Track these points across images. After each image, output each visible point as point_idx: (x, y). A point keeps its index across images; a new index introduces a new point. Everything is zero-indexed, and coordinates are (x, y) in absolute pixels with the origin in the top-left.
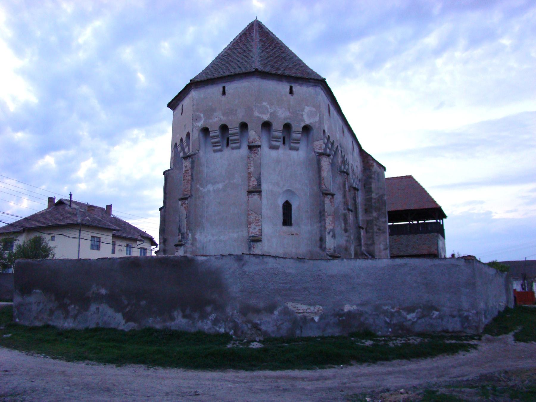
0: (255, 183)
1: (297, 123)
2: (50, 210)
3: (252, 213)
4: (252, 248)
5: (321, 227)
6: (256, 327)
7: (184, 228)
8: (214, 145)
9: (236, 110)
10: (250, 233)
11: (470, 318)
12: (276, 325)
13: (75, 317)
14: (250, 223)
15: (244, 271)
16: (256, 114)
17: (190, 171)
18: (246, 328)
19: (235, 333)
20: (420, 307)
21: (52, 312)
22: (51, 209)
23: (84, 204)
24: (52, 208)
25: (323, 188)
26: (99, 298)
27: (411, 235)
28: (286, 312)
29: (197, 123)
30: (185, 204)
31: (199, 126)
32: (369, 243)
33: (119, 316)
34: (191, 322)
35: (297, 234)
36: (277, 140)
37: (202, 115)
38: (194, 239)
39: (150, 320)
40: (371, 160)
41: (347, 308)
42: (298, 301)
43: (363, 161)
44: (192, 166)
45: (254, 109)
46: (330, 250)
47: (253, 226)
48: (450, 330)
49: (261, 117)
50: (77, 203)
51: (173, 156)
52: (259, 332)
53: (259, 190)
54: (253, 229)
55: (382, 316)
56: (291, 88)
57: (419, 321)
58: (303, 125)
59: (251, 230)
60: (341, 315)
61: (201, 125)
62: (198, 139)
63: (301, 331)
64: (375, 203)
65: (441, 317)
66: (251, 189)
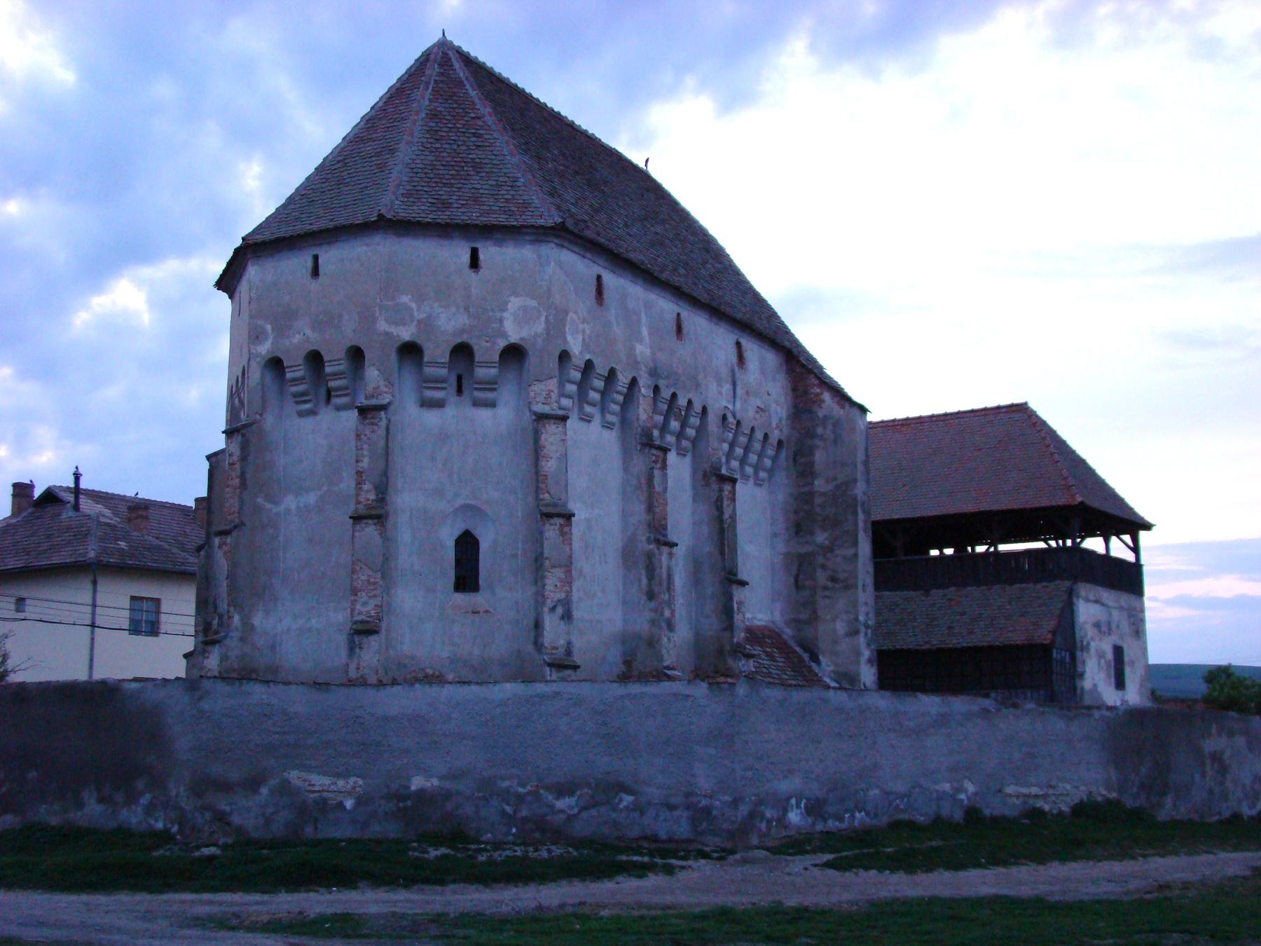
1: (487, 342)
2: (18, 521)
3: (361, 568)
4: (357, 650)
6: (221, 818)
8: (299, 399)
9: (341, 316)
10: (355, 614)
11: (715, 812)
14: (355, 591)
16: (383, 326)
17: (238, 464)
18: (200, 820)
19: (180, 831)
20: (589, 785)
22: (23, 515)
23: (122, 498)
24: (25, 514)
25: (543, 500)
27: (996, 587)
28: (285, 789)
29: (258, 348)
31: (263, 353)
32: (804, 616)
35: (487, 611)
36: (439, 385)
37: (269, 327)
38: (248, 627)
39: (43, 808)
40: (814, 385)
41: (417, 783)
42: (308, 769)
43: (794, 390)
45: (377, 314)
46: (554, 651)
47: (363, 596)
48: (663, 835)
49: (395, 334)
50: (98, 497)
51: (229, 417)
52: (227, 828)
53: (380, 512)
54: (362, 605)
55: (495, 802)
56: (474, 255)
57: (585, 815)
58: (502, 344)
59: (358, 607)
61: (266, 351)
62: (260, 387)
63: (316, 828)
65: (639, 808)
66: (362, 510)
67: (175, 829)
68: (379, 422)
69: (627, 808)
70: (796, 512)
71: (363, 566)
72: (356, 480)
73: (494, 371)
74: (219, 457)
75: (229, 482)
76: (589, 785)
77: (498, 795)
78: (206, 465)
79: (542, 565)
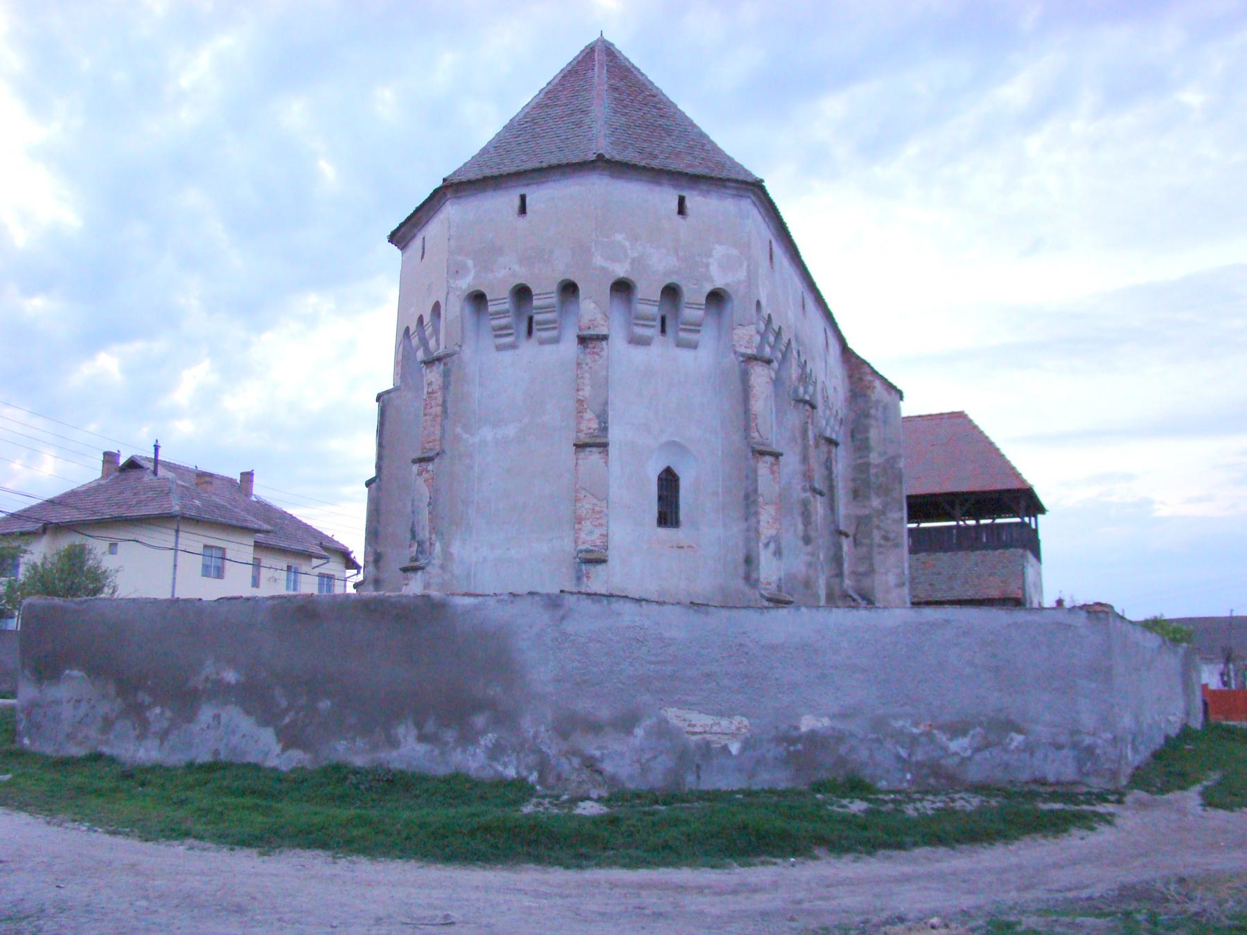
0: (594, 425)
1: (694, 285)
3: (585, 496)
4: (585, 579)
5: (748, 530)
6: (591, 764)
7: (423, 529)
8: (499, 333)
10: (580, 542)
11: (1098, 751)
12: (638, 761)
13: (164, 736)
14: (579, 520)
15: (565, 634)
16: (598, 260)
18: (567, 767)
19: (542, 780)
20: (981, 724)
21: (108, 724)
23: (187, 470)
24: (112, 477)
25: (754, 438)
26: (220, 692)
28: (663, 730)
29: (457, 282)
30: (427, 472)
32: (861, 569)
33: (267, 736)
34: (436, 752)
35: (690, 547)
37: (470, 263)
38: (447, 555)
41: (807, 723)
43: (850, 377)
44: (444, 383)
45: (593, 250)
46: (768, 586)
47: (587, 525)
48: (1051, 778)
49: (611, 269)
51: (400, 357)
52: (599, 778)
53: (603, 440)
54: (587, 534)
55: (889, 744)
56: (682, 201)
57: (978, 757)
58: (708, 288)
59: (583, 535)
60: (792, 741)
62: (459, 319)
63: (699, 777)
64: (876, 475)
65: (1029, 749)
66: (584, 438)
67: (533, 777)
68: (601, 351)
69: (1017, 748)
70: (854, 480)
71: (588, 495)
72: (577, 409)
73: (701, 313)
74: (390, 394)
75: (427, 411)
76: (981, 724)
77: (892, 737)
78: (374, 407)
79: (755, 502)
